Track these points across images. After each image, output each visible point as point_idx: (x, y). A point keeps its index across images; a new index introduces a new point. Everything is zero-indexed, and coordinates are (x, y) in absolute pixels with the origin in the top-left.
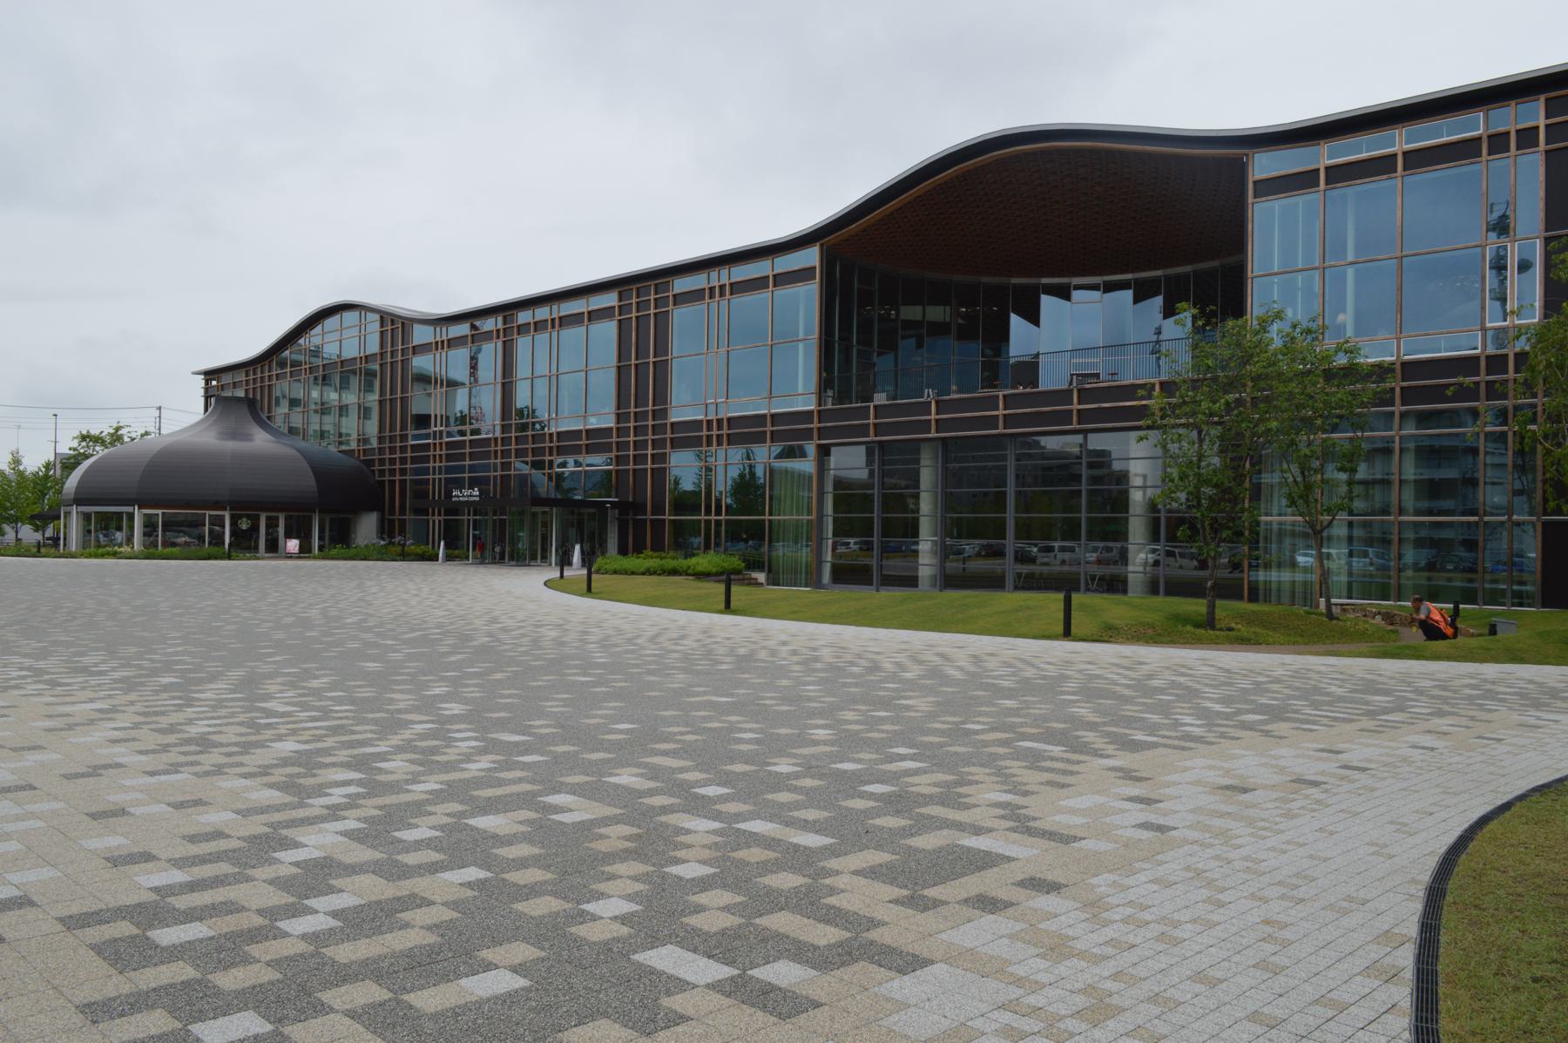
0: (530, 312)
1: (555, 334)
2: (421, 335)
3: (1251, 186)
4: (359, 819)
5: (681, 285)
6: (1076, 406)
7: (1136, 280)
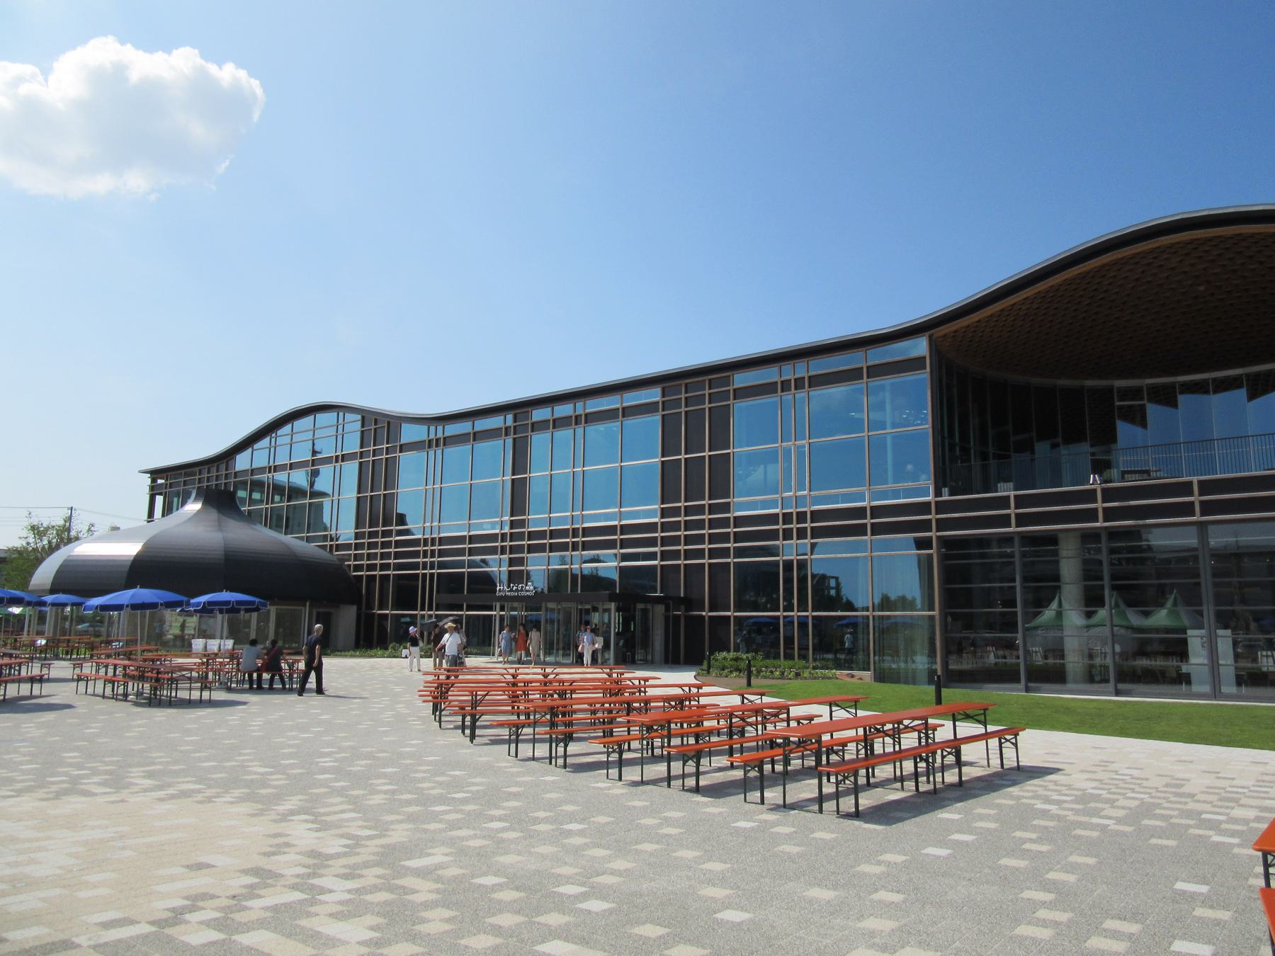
0: (571, 406)
1: (439, 452)
2: (410, 433)
4: (251, 909)
5: (741, 379)
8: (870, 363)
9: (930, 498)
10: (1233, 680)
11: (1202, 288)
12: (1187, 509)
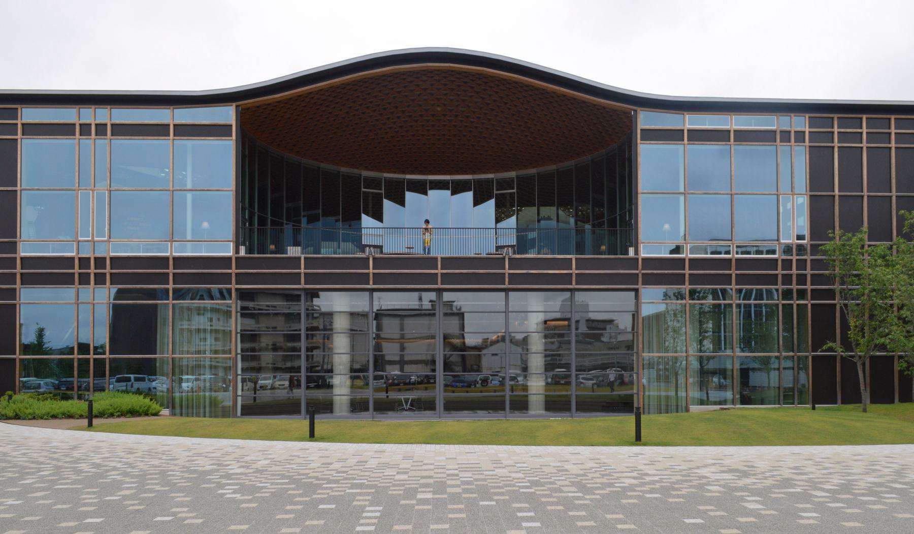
3: (639, 132)
5: (30, 115)
6: (507, 271)
7: (453, 182)
8: (177, 122)
9: (230, 253)
10: (542, 405)
11: (439, 109)
12: (432, 278)
